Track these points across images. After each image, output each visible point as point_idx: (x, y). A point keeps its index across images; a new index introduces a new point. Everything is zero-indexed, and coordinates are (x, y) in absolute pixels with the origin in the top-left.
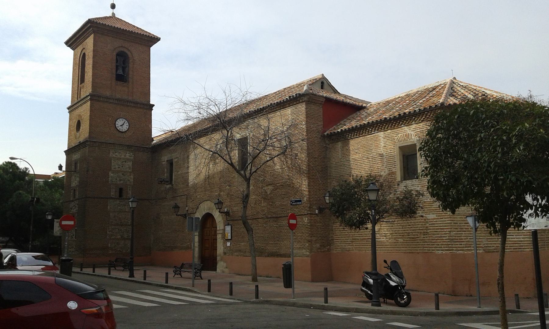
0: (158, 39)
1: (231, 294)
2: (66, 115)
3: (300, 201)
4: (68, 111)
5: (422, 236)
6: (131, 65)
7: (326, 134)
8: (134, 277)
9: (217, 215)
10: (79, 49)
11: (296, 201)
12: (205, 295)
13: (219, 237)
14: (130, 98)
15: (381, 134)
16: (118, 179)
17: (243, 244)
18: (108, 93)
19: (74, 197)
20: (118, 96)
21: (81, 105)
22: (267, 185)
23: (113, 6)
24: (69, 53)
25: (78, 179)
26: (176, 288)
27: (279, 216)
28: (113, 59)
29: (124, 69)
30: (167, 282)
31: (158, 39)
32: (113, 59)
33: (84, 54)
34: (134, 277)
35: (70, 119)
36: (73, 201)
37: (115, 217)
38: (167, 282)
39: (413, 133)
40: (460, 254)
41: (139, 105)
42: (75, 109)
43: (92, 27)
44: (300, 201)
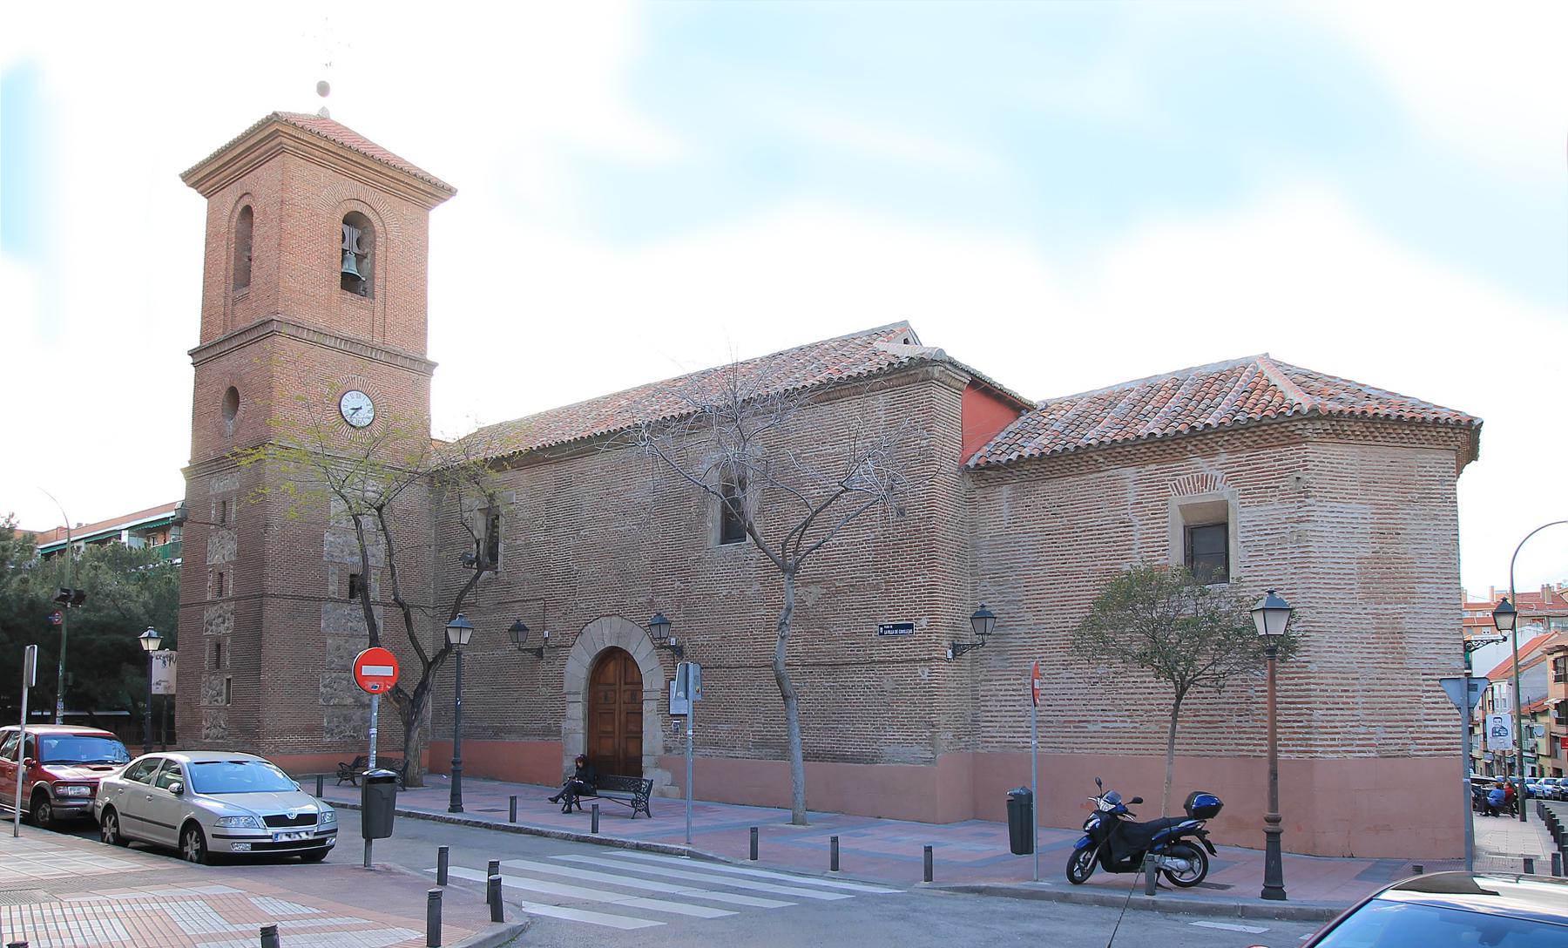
0: (449, 192)
1: (754, 856)
2: (189, 372)
3: (910, 626)
4: (190, 360)
5: (1235, 719)
6: (380, 252)
7: (971, 463)
8: (1282, 897)
9: (642, 652)
10: (230, 196)
11: (896, 627)
12: (741, 866)
13: (650, 709)
14: (378, 340)
15: (1130, 473)
16: (347, 551)
17: (725, 727)
18: (320, 322)
19: (220, 593)
20: (347, 332)
21: (241, 346)
22: (805, 585)
23: (323, 89)
24: (196, 206)
25: (232, 546)
26: (638, 848)
27: (840, 661)
28: (304, 233)
29: (360, 258)
30: (513, 819)
31: (449, 192)
32: (304, 233)
33: (248, 211)
34: (1282, 897)
35: (199, 384)
36: (214, 603)
37: (338, 649)
38: (513, 819)
39: (1219, 474)
40: (1331, 760)
41: (399, 361)
42: (218, 356)
43: (270, 141)
44: (910, 626)
